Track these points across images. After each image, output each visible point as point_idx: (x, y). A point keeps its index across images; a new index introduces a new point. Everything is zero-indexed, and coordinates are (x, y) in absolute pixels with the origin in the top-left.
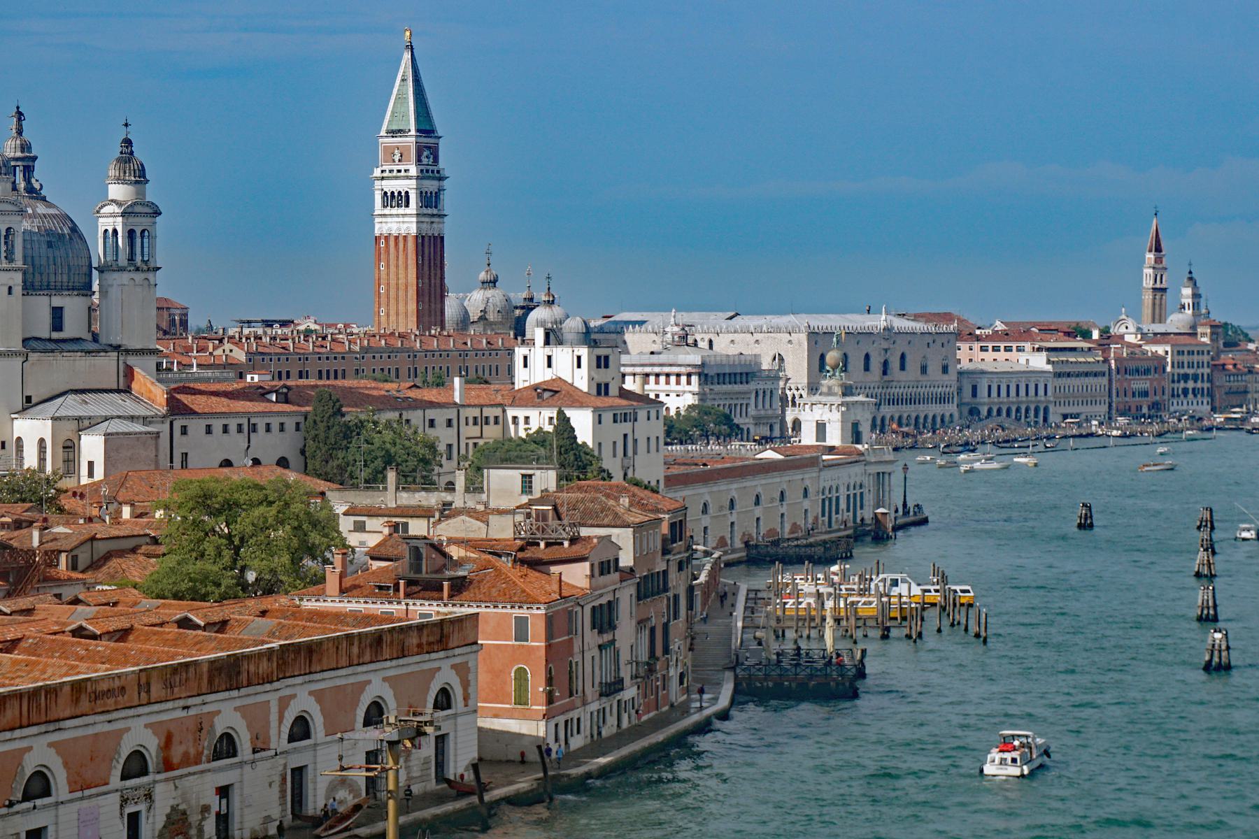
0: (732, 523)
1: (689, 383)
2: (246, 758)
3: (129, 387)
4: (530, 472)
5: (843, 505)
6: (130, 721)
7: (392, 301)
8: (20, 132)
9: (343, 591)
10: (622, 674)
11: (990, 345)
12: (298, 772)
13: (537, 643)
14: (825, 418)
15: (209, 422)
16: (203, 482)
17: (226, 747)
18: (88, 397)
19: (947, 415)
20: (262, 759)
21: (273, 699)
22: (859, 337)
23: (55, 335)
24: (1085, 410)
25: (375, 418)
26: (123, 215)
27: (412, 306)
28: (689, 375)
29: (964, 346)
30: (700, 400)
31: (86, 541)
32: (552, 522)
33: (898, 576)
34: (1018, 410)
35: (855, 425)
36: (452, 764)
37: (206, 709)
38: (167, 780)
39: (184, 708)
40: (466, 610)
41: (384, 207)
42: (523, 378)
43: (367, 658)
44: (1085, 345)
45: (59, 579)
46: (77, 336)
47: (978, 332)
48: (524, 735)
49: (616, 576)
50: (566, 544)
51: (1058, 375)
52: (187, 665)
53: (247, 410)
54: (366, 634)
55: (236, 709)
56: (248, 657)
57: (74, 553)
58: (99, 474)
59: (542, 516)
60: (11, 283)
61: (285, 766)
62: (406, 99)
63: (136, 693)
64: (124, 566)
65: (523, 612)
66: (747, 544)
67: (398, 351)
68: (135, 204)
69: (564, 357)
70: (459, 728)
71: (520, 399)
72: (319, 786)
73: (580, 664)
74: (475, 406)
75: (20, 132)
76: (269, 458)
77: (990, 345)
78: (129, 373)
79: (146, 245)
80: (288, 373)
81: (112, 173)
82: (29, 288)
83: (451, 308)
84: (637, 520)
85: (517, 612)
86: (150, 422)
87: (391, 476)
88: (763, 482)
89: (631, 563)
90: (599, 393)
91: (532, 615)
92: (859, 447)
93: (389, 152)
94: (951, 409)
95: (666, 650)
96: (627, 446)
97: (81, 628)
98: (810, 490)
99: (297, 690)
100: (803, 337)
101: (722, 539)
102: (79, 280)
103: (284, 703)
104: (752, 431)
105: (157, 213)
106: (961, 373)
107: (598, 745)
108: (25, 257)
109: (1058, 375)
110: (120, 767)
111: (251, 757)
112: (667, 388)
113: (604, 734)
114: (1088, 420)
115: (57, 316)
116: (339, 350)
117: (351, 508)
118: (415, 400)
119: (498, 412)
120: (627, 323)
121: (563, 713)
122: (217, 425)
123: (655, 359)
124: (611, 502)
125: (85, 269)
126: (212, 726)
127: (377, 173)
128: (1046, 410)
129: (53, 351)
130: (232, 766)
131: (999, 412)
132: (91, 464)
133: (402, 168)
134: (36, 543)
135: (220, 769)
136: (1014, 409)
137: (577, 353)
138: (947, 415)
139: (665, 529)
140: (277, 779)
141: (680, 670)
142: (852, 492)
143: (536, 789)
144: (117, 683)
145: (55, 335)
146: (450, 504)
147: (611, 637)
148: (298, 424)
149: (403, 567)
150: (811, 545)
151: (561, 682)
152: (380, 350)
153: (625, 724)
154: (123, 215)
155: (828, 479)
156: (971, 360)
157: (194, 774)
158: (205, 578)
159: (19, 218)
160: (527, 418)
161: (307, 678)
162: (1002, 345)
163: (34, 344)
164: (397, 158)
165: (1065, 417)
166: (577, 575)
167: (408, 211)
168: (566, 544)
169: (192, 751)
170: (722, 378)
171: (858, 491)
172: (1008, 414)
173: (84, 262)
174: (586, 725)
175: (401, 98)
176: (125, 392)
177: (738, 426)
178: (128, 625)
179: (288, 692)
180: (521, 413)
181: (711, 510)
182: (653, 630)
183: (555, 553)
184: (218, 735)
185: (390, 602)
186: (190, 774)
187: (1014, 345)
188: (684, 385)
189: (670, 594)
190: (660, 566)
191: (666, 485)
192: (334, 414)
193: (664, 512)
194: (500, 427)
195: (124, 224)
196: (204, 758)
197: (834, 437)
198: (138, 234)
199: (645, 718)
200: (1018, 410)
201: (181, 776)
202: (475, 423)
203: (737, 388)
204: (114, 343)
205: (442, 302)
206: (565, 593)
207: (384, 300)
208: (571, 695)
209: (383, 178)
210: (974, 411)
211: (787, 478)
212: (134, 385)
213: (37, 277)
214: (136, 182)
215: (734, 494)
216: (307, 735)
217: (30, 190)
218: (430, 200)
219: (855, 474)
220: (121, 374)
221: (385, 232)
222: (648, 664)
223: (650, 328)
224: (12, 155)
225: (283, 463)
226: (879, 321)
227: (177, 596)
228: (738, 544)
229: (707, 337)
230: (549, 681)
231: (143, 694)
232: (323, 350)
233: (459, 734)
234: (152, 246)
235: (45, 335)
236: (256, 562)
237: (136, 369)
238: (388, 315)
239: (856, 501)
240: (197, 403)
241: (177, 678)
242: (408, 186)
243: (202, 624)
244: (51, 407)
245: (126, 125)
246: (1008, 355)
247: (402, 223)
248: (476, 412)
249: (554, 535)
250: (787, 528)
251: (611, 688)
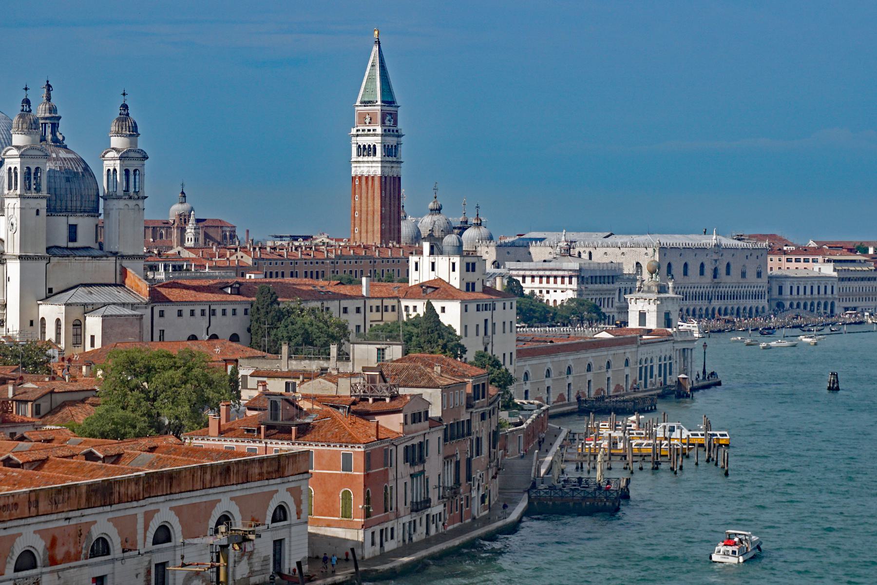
0: (569, 384)
1: (570, 283)
2: (116, 556)
3: (124, 282)
4: (383, 347)
5: (656, 371)
6: (22, 528)
7: (364, 223)
8: (49, 99)
9: (221, 433)
10: (430, 496)
11: (794, 258)
12: (162, 567)
13: (358, 473)
14: (645, 309)
15: (180, 308)
16: (129, 352)
17: (101, 547)
18: (93, 289)
19: (730, 307)
20: (130, 557)
21: (140, 513)
22: (697, 251)
23: (71, 245)
24: (861, 304)
25: (302, 306)
26: (121, 158)
27: (377, 227)
28: (570, 277)
29: (776, 258)
30: (578, 295)
31: (47, 394)
32: (379, 384)
33: (675, 425)
34: (812, 304)
35: (667, 314)
36: (287, 561)
37: (84, 520)
38: (52, 572)
39: (66, 519)
40: (306, 448)
41: (359, 156)
42: (414, 278)
43: (218, 483)
44: (862, 258)
45: (14, 422)
46: (87, 245)
47: (785, 248)
48: (348, 540)
49: (427, 423)
50: (388, 400)
51: (842, 279)
52: (69, 488)
53: (209, 299)
54: (217, 465)
55: (109, 520)
56: (116, 481)
57: (37, 402)
58: (98, 344)
59: (372, 379)
60: (38, 207)
61: (150, 562)
62: (374, 79)
63: (27, 508)
64: (73, 412)
65: (348, 450)
66: (578, 398)
67: (363, 258)
68: (32, 148)
69: (443, 263)
70: (293, 535)
71: (411, 294)
72: (177, 577)
73: (394, 488)
74: (377, 298)
75: (49, 99)
76: (225, 334)
77: (794, 258)
78: (124, 273)
79: (137, 180)
80: (283, 273)
81: (113, 128)
82: (51, 210)
83: (406, 229)
84: (446, 383)
85: (344, 450)
86: (137, 308)
87: (285, 349)
88: (594, 354)
89: (440, 415)
90: (468, 290)
91: (355, 452)
92: (669, 330)
93: (362, 116)
94: (763, 303)
95: (469, 478)
96: (487, 328)
97: (9, 458)
98: (631, 361)
99: (160, 506)
101: (561, 395)
102: (89, 205)
103: (149, 517)
104: (616, 317)
105: (145, 158)
106: (771, 278)
107: (408, 547)
108: (49, 189)
109: (842, 279)
110: (14, 562)
111: (122, 555)
112: (555, 286)
113: (414, 539)
114: (863, 312)
115: (73, 231)
116: (320, 257)
117: (256, 371)
118: (334, 293)
119: (394, 302)
120: (531, 239)
121: (378, 524)
122: (186, 310)
123: (546, 265)
124: (429, 370)
125: (93, 198)
126: (89, 532)
127: (354, 131)
128: (832, 304)
129: (68, 256)
130: (106, 562)
131: (798, 306)
132: (93, 337)
133: (371, 128)
134: (10, 395)
135: (96, 564)
136: (809, 304)
137: (452, 261)
138: (761, 307)
139: (469, 389)
140: (143, 572)
141: (481, 492)
142: (663, 362)
143: (350, 580)
144: (11, 500)
145: (71, 245)
146: (326, 369)
147: (421, 469)
148: (246, 310)
149: (266, 416)
150: (624, 401)
151: (377, 501)
152: (349, 258)
153: (433, 532)
154: (121, 158)
155: (644, 353)
156: (780, 268)
157: (74, 567)
158: (125, 422)
159: (45, 160)
160: (415, 307)
161: (168, 497)
162: (802, 258)
163: (55, 251)
164: (368, 121)
165: (846, 309)
166: (394, 423)
167: (375, 159)
168: (388, 400)
169: (73, 551)
170: (594, 279)
171: (668, 362)
172: (805, 307)
173: (93, 192)
174: (399, 533)
175: (371, 79)
176: (120, 285)
177: (604, 314)
178: (45, 457)
179: (152, 508)
180: (411, 304)
181: (552, 375)
182: (458, 464)
183: (380, 406)
184: (94, 539)
185: (254, 442)
186: (70, 568)
187: (811, 258)
188: (567, 284)
189: (474, 437)
190: (465, 417)
191: (518, 356)
192: (272, 303)
193: (469, 377)
194: (396, 313)
195: (121, 165)
196: (82, 556)
197: (652, 323)
198: (132, 172)
199: (450, 528)
200: (812, 304)
201: (64, 570)
202: (378, 311)
203: (605, 286)
204: (113, 251)
205: (399, 224)
206: (381, 436)
207: (357, 222)
208: (386, 511)
209: (358, 136)
210: (780, 305)
211: (613, 352)
212: (127, 281)
213: (59, 203)
214: (130, 135)
215: (571, 363)
216: (168, 539)
217: (55, 140)
218: (390, 151)
219: (666, 349)
220: (118, 273)
221: (359, 174)
222: (452, 488)
223: (547, 243)
224: (43, 115)
225: (234, 338)
226: (712, 240)
227: (104, 435)
228: (573, 399)
229: (587, 250)
230: (367, 500)
231: (33, 509)
232: (307, 257)
233: (293, 539)
234: (142, 182)
235: (63, 244)
236: (166, 411)
237: (129, 270)
238: (360, 232)
239: (666, 369)
240: (173, 294)
241: (61, 497)
242: (376, 141)
243: (102, 456)
244: (65, 297)
245: (124, 94)
246: (806, 265)
247: (371, 167)
248: (378, 302)
249: (379, 394)
250: (612, 388)
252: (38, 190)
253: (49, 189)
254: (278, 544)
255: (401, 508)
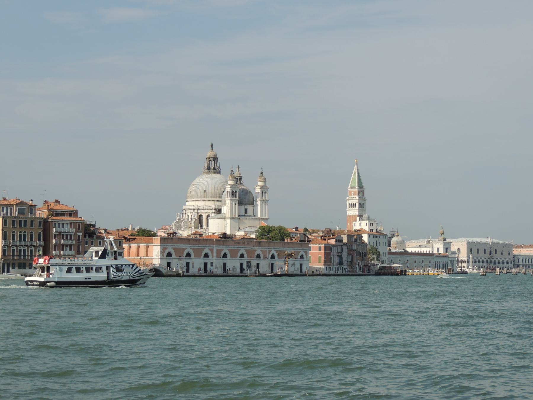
13: (322, 251)
26: (261, 188)
69: (363, 223)
93: (351, 192)
100: (466, 243)
103: (270, 251)
175: (354, 178)
197: (441, 251)
217: (240, 183)
218: (361, 206)
219: (445, 260)
242: (356, 202)
244: (244, 230)
251: (341, 264)
252: (235, 197)
253: (239, 198)
254: (301, 265)
255: (335, 264)
